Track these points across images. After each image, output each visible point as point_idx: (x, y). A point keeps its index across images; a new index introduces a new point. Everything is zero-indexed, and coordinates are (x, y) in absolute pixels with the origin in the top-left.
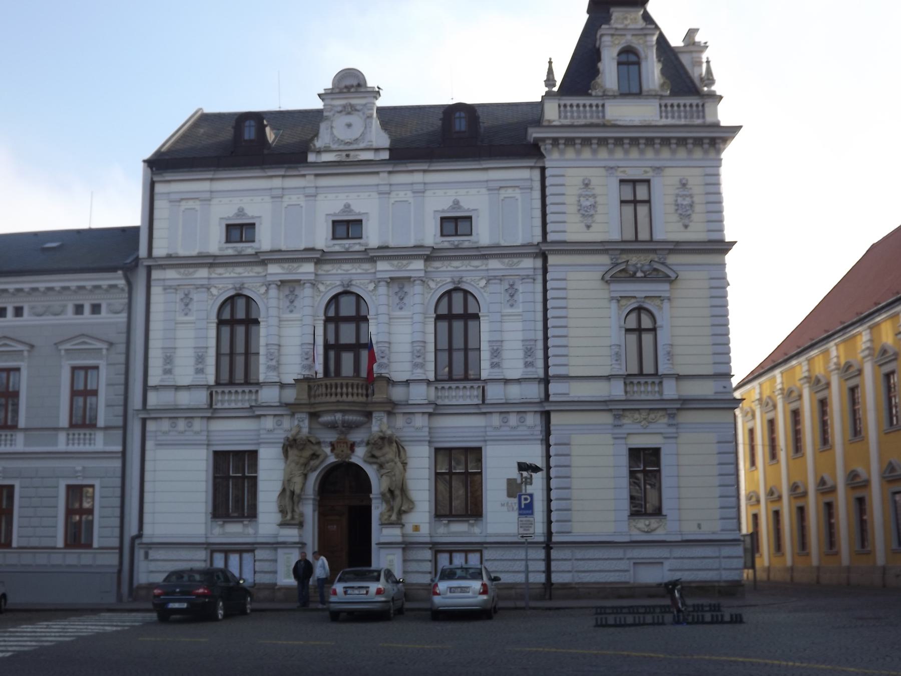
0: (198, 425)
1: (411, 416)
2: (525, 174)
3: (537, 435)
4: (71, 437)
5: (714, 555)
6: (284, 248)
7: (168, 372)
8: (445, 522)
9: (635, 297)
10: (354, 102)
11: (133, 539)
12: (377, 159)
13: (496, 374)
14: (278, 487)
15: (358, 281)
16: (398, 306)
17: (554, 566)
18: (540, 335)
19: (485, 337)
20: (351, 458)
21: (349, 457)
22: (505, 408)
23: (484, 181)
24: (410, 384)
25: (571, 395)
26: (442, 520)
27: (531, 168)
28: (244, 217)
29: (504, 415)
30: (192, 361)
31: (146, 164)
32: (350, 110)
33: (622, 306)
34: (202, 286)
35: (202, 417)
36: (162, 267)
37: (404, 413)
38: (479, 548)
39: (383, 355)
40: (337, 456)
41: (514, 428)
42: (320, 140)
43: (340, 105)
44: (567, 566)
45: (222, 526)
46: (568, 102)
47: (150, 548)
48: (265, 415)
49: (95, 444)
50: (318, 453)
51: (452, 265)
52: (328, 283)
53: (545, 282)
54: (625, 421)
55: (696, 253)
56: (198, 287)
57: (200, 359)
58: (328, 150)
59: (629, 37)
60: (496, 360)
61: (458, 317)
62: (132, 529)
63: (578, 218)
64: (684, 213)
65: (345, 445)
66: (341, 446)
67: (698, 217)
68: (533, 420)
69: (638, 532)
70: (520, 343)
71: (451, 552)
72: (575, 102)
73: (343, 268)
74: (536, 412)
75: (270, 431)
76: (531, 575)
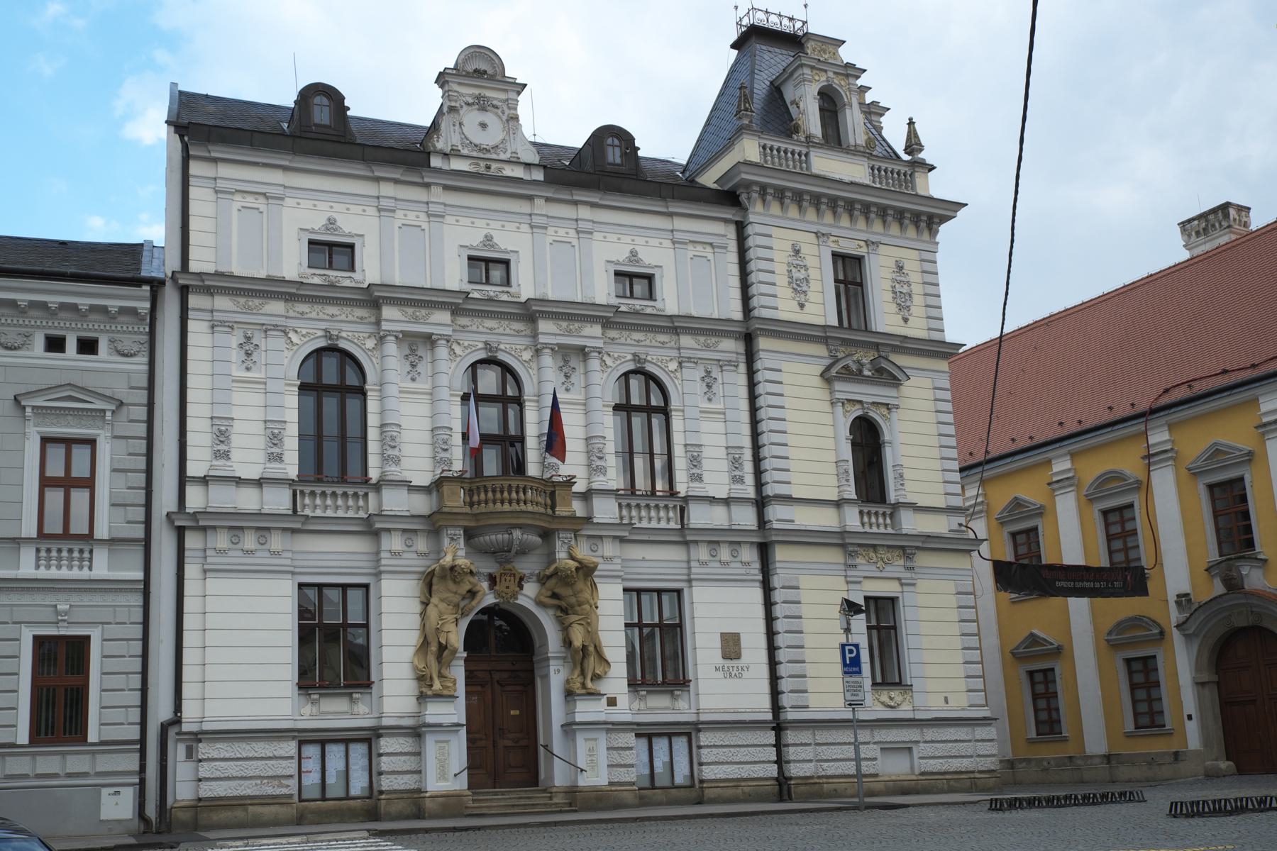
1: (598, 542)
2: (719, 228)
4: (43, 554)
5: (967, 738)
6: (551, 297)
7: (697, 478)
8: (316, 697)
9: (860, 402)
10: (489, 94)
11: (164, 728)
12: (527, 177)
14: (414, 638)
16: (245, 365)
17: (772, 754)
18: (747, 442)
20: (517, 599)
21: (515, 596)
22: (715, 538)
24: (210, 483)
25: (796, 522)
27: (726, 221)
30: (261, 442)
31: (172, 129)
32: (482, 104)
33: (847, 411)
36: (209, 291)
37: (589, 537)
38: (689, 731)
39: (393, 444)
40: (498, 595)
41: (249, 552)
42: (441, 140)
43: (470, 95)
44: (836, 752)
45: (314, 702)
46: (769, 143)
47: (200, 741)
48: (214, 528)
49: (90, 568)
50: (474, 589)
51: (326, 311)
52: (466, 344)
53: (751, 373)
54: (859, 560)
55: (804, 341)
56: (266, 330)
57: (275, 439)
59: (831, 74)
61: (331, 389)
62: (161, 710)
63: (788, 292)
64: (902, 301)
65: (512, 578)
67: (917, 310)
68: (750, 555)
69: (880, 707)
71: (323, 743)
72: (776, 145)
73: (298, 309)
74: (752, 543)
76: (864, 763)
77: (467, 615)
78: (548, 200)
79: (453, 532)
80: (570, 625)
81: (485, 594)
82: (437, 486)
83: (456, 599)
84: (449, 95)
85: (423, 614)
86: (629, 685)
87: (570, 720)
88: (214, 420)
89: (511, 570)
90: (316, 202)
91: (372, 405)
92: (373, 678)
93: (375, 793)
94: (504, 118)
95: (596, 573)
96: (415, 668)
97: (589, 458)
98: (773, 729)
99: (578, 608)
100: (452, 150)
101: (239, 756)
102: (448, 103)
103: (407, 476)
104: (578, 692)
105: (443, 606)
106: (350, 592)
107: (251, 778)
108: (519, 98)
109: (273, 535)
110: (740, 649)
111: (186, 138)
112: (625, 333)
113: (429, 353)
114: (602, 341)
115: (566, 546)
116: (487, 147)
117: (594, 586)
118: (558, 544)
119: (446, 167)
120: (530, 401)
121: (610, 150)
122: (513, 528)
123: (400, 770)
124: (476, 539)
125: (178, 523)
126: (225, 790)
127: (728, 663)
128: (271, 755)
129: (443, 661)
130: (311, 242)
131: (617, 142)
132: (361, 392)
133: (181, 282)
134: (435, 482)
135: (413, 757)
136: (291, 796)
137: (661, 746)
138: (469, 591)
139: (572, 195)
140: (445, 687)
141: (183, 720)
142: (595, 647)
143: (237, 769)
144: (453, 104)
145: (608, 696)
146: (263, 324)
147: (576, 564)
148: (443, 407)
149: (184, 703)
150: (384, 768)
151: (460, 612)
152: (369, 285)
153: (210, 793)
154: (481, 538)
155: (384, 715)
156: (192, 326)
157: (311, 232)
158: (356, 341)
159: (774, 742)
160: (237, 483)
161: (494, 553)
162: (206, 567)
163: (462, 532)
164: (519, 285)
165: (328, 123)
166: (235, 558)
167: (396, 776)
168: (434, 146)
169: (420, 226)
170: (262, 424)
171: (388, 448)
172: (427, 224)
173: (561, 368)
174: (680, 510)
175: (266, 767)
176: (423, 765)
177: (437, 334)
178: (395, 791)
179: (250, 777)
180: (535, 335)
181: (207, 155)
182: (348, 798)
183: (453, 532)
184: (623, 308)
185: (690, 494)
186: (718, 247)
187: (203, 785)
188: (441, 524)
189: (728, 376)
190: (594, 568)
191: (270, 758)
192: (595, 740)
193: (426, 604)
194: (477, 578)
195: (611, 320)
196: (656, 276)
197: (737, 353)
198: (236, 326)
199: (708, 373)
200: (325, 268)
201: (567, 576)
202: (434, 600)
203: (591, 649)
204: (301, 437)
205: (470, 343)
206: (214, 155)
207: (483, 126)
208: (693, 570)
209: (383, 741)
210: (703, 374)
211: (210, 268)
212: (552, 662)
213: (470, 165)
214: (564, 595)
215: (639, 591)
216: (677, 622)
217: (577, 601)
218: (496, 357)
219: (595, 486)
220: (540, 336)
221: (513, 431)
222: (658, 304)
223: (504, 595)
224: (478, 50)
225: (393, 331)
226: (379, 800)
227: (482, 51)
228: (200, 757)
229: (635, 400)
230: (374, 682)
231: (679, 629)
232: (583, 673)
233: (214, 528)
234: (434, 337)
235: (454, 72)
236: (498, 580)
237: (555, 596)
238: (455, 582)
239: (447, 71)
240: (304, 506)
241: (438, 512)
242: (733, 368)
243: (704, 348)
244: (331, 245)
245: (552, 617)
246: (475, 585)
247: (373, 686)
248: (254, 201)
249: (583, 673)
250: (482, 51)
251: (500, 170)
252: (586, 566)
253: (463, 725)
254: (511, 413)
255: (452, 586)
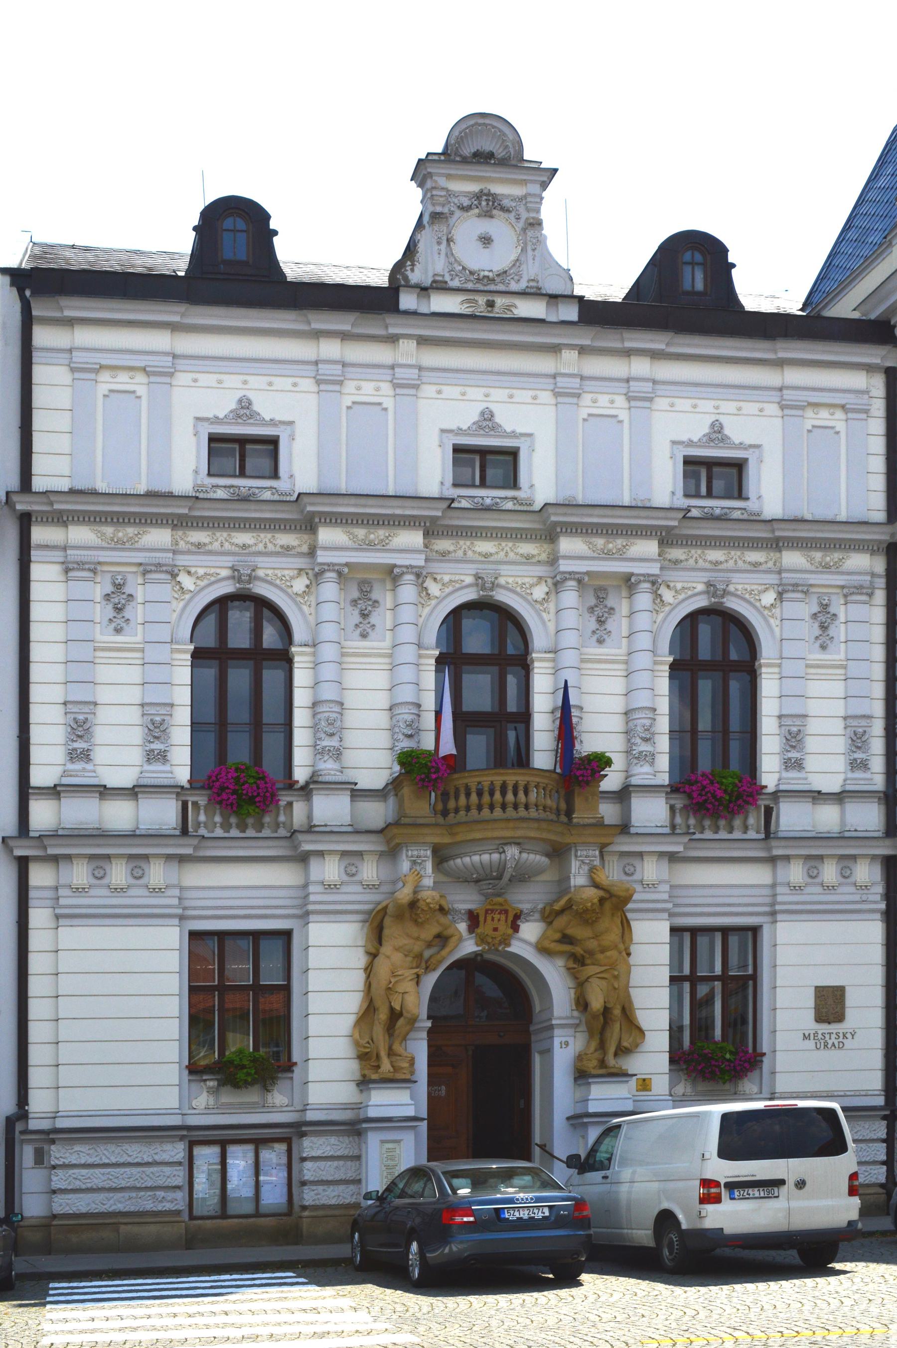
0: (157, 874)
2: (857, 380)
3: (875, 902)
7: (797, 765)
10: (498, 189)
12: (552, 318)
13: (794, 781)
14: (353, 1003)
15: (510, 580)
16: (113, 625)
19: (301, 698)
20: (509, 945)
21: (506, 942)
23: (546, 376)
26: (205, 1080)
27: (869, 368)
28: (251, 421)
29: (813, 863)
30: (136, 735)
34: (159, 567)
35: (169, 857)
36: (61, 519)
39: (330, 730)
40: (481, 940)
41: (119, 890)
43: (466, 194)
44: (328, 1171)
48: (69, 858)
50: (446, 933)
56: (146, 570)
57: (858, 741)
58: (440, 286)
60: (859, 755)
61: (240, 654)
65: (503, 917)
66: (493, 919)
70: (136, 712)
71: (224, 1144)
73: (748, 559)
74: (874, 857)
75: (330, 887)
77: (434, 970)
78: (583, 350)
79: (415, 853)
80: (587, 980)
81: (461, 939)
82: (395, 788)
83: (417, 947)
84: (432, 196)
85: (369, 970)
86: (670, 1061)
87: (579, 1111)
88: (69, 706)
89: (501, 904)
90: (222, 377)
91: (301, 677)
92: (295, 1057)
93: (296, 1208)
94: (521, 224)
95: (630, 906)
96: (357, 1044)
97: (629, 741)
98: (884, 1118)
99: (600, 956)
100: (434, 282)
101: (107, 1161)
102: (431, 209)
103: (350, 775)
104: (594, 1072)
105: (397, 957)
106: (264, 944)
107: (122, 1189)
108: (544, 194)
109: (75, 866)
110: (843, 1007)
111: (28, 293)
112: (696, 552)
113: (389, 596)
114: (658, 565)
115: (586, 868)
116: (491, 274)
117: (626, 925)
118: (574, 865)
119: (424, 309)
120: (541, 660)
121: (687, 270)
122: (506, 844)
123: (330, 1178)
124: (451, 863)
125: (18, 852)
126: (88, 1204)
127: (824, 1028)
128: (150, 1160)
129: (397, 1032)
130: (457, 449)
131: (698, 257)
132: (284, 659)
133: (19, 507)
134: (391, 783)
135: (349, 1163)
136: (178, 1213)
137: (207, 1156)
138: (438, 936)
139: (623, 341)
140: (396, 1069)
141: (31, 1116)
142: (624, 1009)
143: (104, 1178)
144: (439, 209)
145: (638, 1077)
146: (141, 564)
147: (601, 893)
148: (642, 679)
149: (32, 1093)
150: (308, 1176)
151: (423, 965)
152: (299, 494)
153: (119, 1205)
154: (459, 861)
155: (308, 1107)
156: (37, 571)
157: (212, 423)
158: (278, 582)
159: (884, 1136)
160: (814, 798)
161: (477, 881)
162: (58, 911)
163: (429, 853)
164: (532, 486)
165: (244, 258)
166: (99, 897)
167: (325, 1187)
168: (406, 278)
169: (380, 404)
170: (61, 708)
171: (323, 736)
172: (844, 423)
173: (591, 610)
174: (765, 811)
175: (144, 1176)
176: (364, 1171)
177: (401, 566)
178: (324, 1207)
179: (122, 1188)
180: (553, 560)
181: (57, 314)
182: (257, 1214)
183: (415, 853)
184: (695, 513)
185: (782, 787)
186: (155, 374)
187: (58, 1199)
188: (397, 841)
189: (857, 611)
190: (628, 899)
191: (148, 1164)
192: (398, 1142)
193: (373, 955)
194: (450, 917)
195: (677, 531)
196: (750, 461)
197: (873, 575)
198: (99, 568)
199: (824, 607)
200: (234, 476)
201: (586, 911)
202: (386, 949)
203: (617, 1012)
204: (196, 726)
205: (686, 585)
206: (68, 313)
207: (486, 240)
208: (779, 898)
209: (307, 1142)
210: (815, 608)
211: (64, 485)
212: (557, 1032)
213: (462, 303)
214: (579, 938)
215: (695, 931)
216: (750, 971)
217: (599, 945)
218: (722, 603)
219: (635, 781)
220: (561, 562)
221: (512, 706)
222: (751, 505)
223: (490, 940)
224: (481, 121)
225: (334, 565)
226: (301, 1217)
227: (487, 121)
228: (53, 1163)
229: (705, 652)
230: (296, 1064)
231: (751, 983)
232: (602, 1046)
233: (69, 858)
234: (396, 570)
235: (442, 158)
236: (481, 919)
237: (566, 939)
238: (416, 922)
239: (430, 158)
240: (198, 825)
241: (397, 824)
242: (864, 598)
243: (820, 569)
244: (243, 441)
245: (563, 970)
246: (446, 928)
247: (294, 1068)
248: (830, 417)
249: (602, 1046)
250: (487, 121)
251: (508, 308)
252: (615, 896)
253: (423, 1119)
254: (734, 686)
255: (414, 931)
